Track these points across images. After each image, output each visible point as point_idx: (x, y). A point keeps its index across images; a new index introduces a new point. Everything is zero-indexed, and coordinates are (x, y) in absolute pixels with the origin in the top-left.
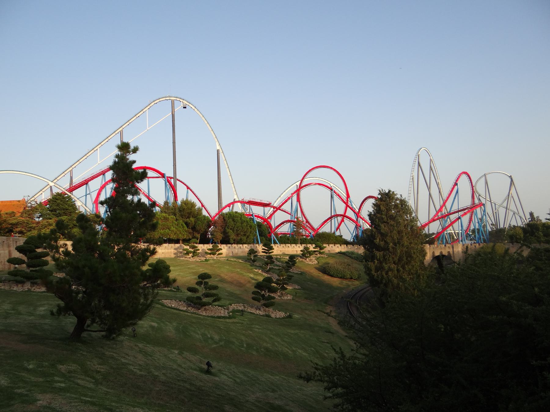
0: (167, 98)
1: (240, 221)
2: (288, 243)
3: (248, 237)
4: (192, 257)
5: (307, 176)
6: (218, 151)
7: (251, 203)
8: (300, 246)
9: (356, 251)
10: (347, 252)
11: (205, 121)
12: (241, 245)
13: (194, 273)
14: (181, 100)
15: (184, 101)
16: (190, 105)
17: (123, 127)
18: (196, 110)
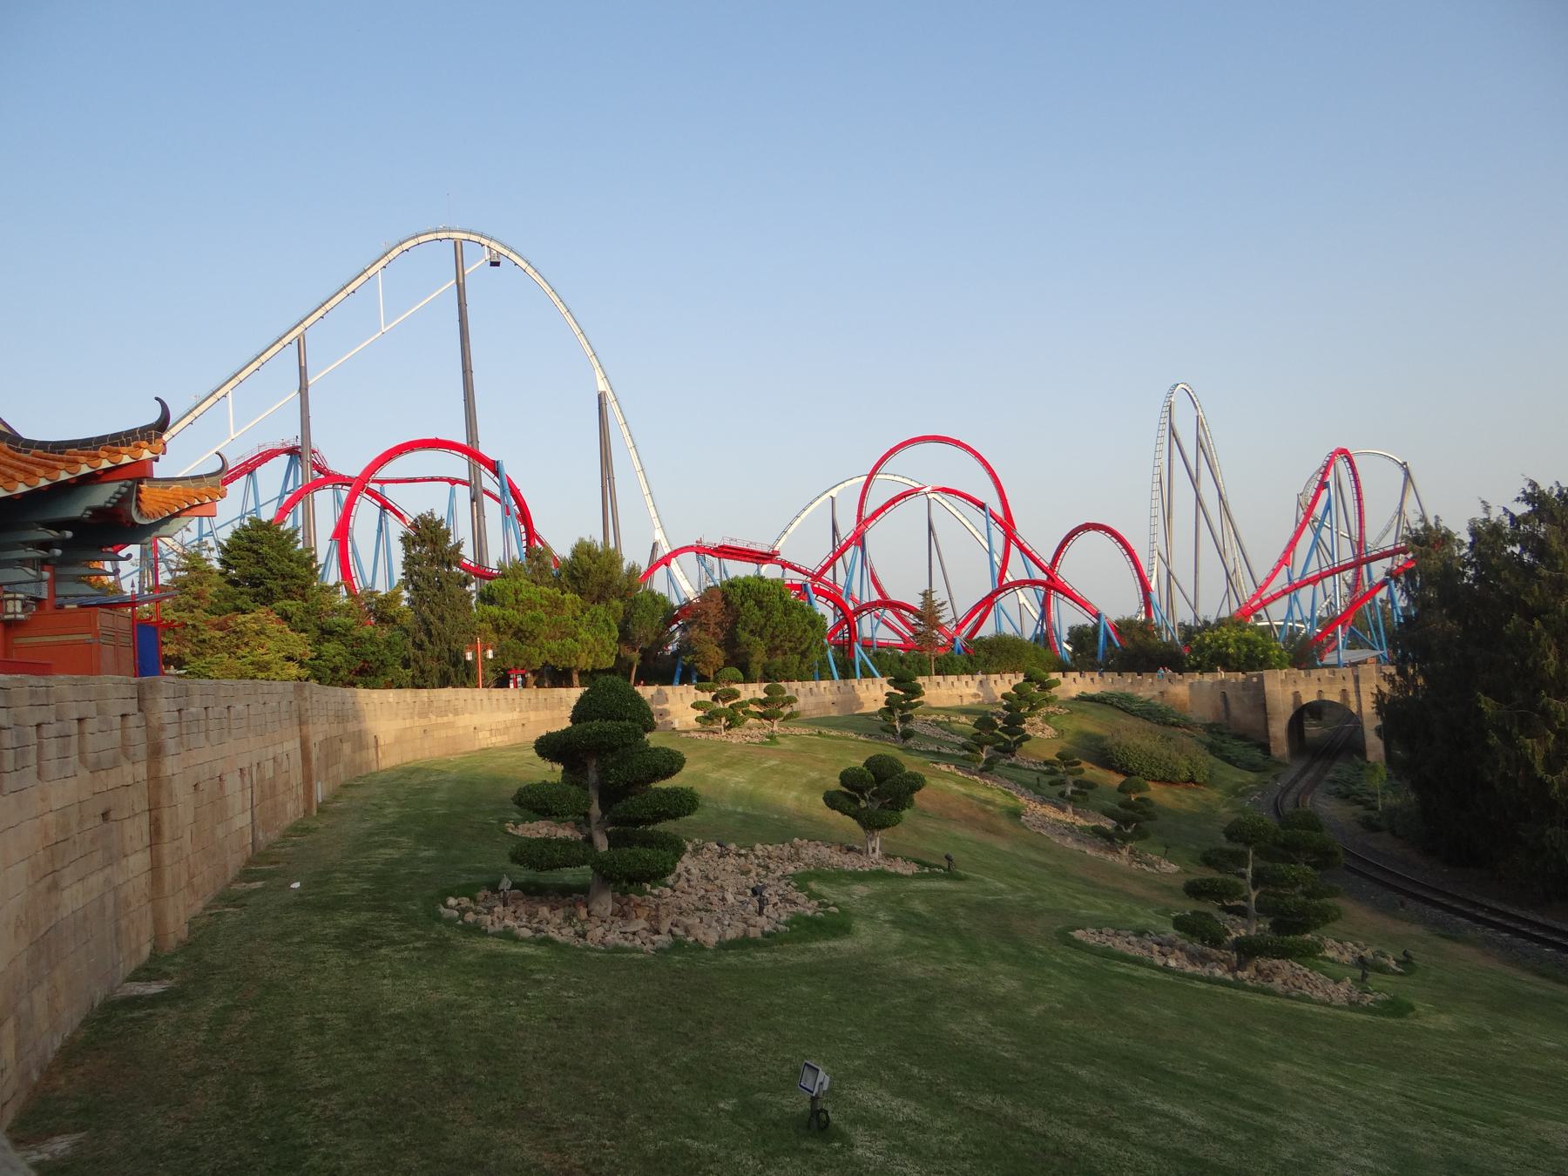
0: (440, 236)
1: (780, 606)
2: (1093, 670)
3: (803, 654)
4: (728, 728)
5: (884, 468)
6: (601, 398)
7: (725, 552)
8: (1079, 679)
9: (1129, 690)
10: (1112, 695)
11: (560, 306)
12: (812, 684)
13: (811, 786)
14: (483, 241)
15: (492, 245)
16: (512, 256)
17: (307, 323)
18: (530, 270)
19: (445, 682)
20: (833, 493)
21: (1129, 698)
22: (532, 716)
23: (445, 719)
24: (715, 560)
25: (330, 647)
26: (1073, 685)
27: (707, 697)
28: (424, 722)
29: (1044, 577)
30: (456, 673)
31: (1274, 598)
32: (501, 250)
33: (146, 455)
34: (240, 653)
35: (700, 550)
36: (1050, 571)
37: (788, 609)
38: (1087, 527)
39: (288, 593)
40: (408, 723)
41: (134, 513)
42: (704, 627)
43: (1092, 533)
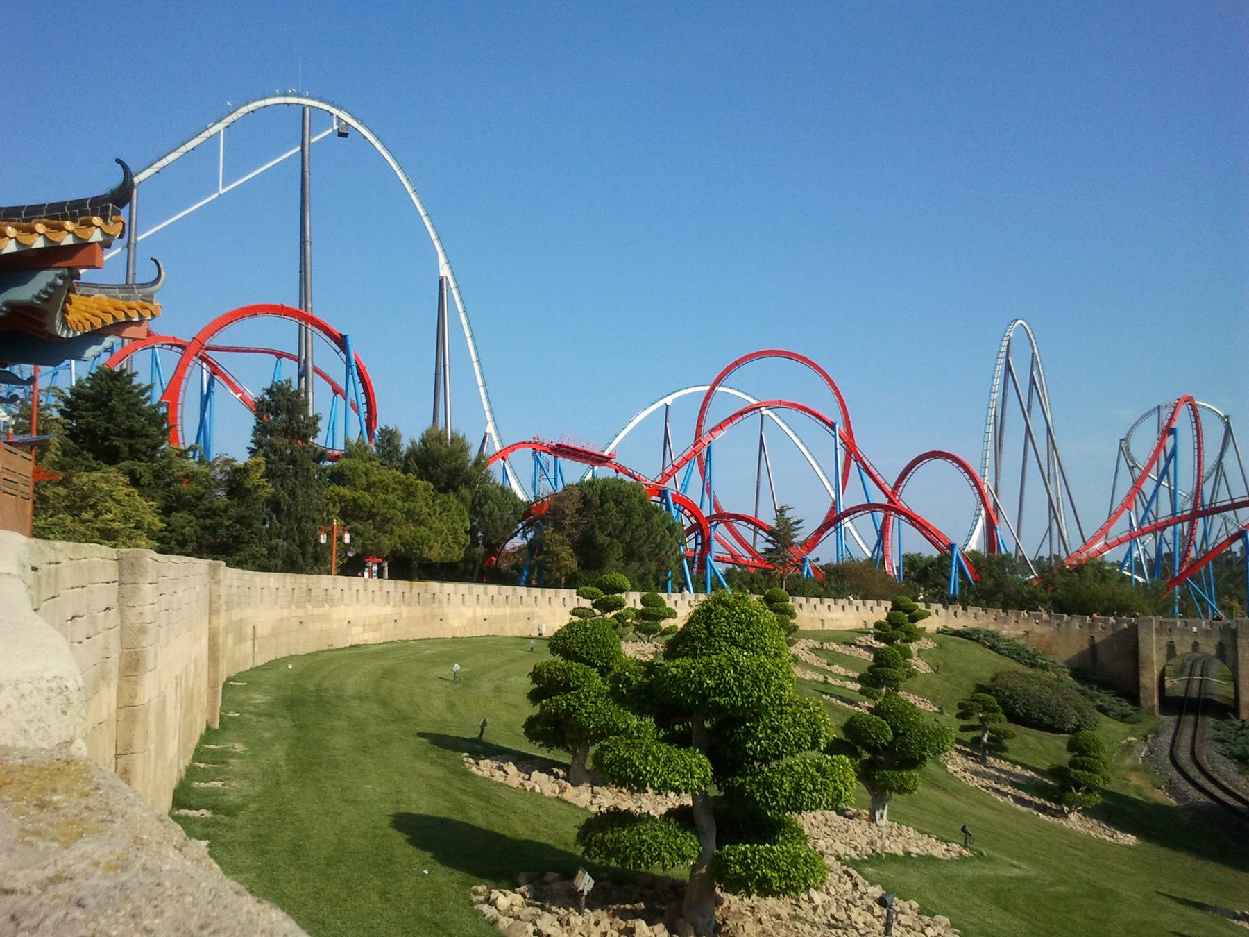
19: (291, 566)
20: (668, 400)
21: (994, 635)
22: (405, 611)
23: (321, 611)
24: (551, 458)
25: (178, 518)
26: (936, 619)
27: (587, 603)
28: (300, 612)
31: (1120, 542)
33: (96, 236)
34: (85, 516)
35: (537, 447)
36: (893, 494)
37: (650, 512)
39: (134, 454)
40: (285, 613)
41: (58, 321)
43: (939, 461)
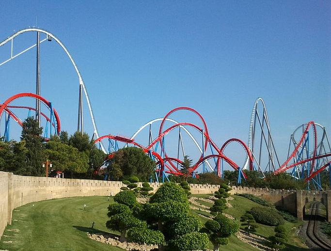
7: (117, 138)
20: (151, 123)
24: (114, 141)
26: (234, 191)
27: (125, 186)
28: (37, 189)
29: (218, 154)
30: (37, 172)
32: (52, 36)
35: (110, 137)
37: (145, 158)
38: (233, 140)
40: (32, 189)
42: (117, 162)
